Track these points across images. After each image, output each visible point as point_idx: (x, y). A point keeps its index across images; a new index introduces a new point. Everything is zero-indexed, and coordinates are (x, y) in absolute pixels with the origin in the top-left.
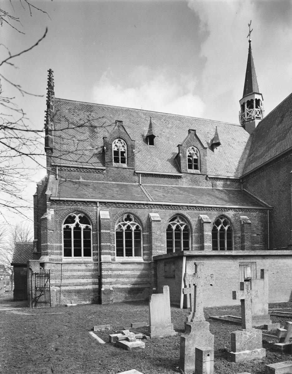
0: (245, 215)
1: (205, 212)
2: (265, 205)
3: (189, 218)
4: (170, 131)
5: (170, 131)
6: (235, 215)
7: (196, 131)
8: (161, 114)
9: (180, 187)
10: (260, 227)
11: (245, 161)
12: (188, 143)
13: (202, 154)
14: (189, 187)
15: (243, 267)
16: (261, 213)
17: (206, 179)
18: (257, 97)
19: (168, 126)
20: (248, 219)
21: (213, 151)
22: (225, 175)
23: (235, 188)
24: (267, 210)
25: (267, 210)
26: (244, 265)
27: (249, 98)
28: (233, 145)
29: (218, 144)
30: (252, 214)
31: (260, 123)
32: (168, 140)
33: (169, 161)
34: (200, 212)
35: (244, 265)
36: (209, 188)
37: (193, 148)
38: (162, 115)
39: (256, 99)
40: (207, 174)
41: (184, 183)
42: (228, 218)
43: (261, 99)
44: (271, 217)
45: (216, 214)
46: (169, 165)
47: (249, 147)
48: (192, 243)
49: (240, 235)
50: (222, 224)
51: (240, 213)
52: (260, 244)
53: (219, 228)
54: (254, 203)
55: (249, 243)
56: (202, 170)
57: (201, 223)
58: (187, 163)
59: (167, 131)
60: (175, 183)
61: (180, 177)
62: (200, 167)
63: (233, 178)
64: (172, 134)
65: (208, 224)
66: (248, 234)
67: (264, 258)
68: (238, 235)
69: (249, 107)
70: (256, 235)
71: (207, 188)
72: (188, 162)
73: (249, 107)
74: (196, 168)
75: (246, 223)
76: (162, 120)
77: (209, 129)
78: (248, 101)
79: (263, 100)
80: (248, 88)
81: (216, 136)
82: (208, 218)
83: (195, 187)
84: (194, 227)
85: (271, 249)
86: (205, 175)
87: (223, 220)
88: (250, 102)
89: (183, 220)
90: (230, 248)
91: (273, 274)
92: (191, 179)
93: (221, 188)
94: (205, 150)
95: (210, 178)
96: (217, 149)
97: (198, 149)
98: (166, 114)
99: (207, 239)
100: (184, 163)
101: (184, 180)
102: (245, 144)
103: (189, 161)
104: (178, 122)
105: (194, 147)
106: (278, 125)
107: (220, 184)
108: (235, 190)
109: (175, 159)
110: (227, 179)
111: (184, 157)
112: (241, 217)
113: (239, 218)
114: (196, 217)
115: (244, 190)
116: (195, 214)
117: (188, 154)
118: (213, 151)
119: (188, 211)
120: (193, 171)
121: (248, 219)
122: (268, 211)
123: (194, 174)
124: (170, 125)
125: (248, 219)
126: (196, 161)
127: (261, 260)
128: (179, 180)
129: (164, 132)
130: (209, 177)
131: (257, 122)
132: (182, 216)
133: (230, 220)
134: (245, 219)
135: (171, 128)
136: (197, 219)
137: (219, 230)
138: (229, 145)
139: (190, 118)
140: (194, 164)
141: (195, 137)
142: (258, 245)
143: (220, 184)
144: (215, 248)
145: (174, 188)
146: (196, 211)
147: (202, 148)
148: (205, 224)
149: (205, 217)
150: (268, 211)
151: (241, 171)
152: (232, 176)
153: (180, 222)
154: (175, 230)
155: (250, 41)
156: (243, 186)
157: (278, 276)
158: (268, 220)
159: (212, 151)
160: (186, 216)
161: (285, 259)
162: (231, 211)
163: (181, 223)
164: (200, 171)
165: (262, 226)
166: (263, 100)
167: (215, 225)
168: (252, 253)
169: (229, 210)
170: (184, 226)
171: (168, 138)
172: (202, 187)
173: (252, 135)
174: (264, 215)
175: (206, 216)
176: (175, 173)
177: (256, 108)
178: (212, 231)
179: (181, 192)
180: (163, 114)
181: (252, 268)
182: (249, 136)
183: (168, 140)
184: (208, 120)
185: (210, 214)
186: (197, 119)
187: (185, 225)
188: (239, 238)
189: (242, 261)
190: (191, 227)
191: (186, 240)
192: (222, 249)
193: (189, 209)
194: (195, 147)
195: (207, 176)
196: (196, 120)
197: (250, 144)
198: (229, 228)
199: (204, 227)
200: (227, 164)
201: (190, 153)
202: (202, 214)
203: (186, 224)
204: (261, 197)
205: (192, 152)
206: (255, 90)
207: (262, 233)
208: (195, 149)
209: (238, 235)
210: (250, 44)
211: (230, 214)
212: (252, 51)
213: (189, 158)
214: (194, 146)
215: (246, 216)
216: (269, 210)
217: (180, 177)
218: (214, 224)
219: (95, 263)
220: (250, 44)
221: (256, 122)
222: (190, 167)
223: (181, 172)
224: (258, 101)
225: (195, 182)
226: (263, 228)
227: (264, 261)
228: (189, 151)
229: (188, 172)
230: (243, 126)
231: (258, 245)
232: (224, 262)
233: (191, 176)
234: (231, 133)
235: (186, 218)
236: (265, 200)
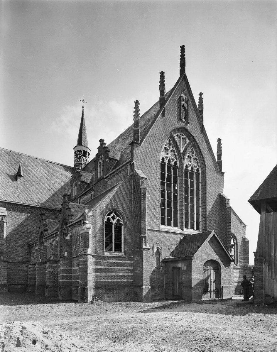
39: (84, 151)
43: (89, 151)
96: (20, 179)
155: (83, 107)
210: (83, 109)
220: (83, 109)
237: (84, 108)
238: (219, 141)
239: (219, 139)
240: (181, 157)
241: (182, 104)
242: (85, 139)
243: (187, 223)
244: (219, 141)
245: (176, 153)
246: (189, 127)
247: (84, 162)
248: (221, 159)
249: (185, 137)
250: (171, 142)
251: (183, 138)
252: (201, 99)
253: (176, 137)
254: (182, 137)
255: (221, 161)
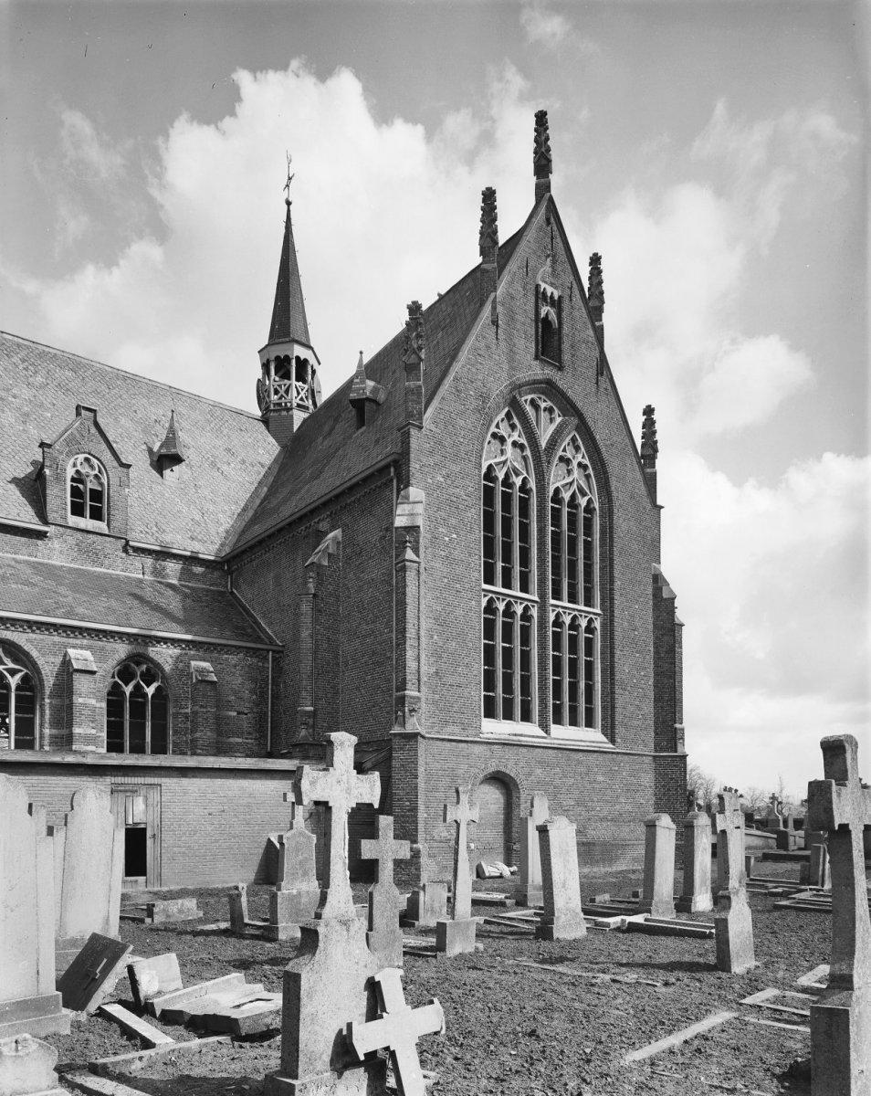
0: (204, 660)
1: (85, 642)
2: (270, 637)
3: (34, 654)
4: (35, 396)
5: (35, 396)
6: (178, 659)
7: (99, 415)
8: (16, 339)
9: (40, 563)
10: (246, 694)
11: (251, 513)
12: (73, 445)
13: (114, 481)
14: (72, 565)
15: (121, 795)
16: (251, 657)
17: (125, 551)
18: (299, 351)
19: (31, 379)
20: (212, 672)
21: (162, 476)
22: (183, 545)
23: (211, 585)
24: (268, 651)
25: (268, 651)
26: (126, 791)
27: (280, 351)
28: (225, 468)
29: (176, 459)
30: (227, 660)
31: (305, 421)
32: (24, 422)
33: (17, 485)
34: (71, 641)
35: (126, 791)
36: (130, 575)
37: (87, 460)
38: (19, 345)
39: (298, 358)
40: (128, 538)
41: (56, 552)
42: (158, 665)
43: (312, 361)
44: (278, 670)
45: (122, 650)
46: (14, 497)
47: (271, 479)
48: (42, 725)
49: (189, 711)
50: (138, 678)
51: (192, 652)
52: (247, 739)
53: (128, 689)
54: (244, 629)
55: (209, 734)
56: (113, 524)
57: (67, 671)
58: (69, 499)
59: (26, 393)
60: (24, 550)
61: (41, 535)
62: (108, 515)
63: (212, 558)
64: (41, 405)
65: (88, 676)
66: (209, 709)
67: (185, 776)
68: (183, 711)
69: (280, 374)
70: (235, 714)
71: (127, 574)
72: (72, 496)
73: (280, 374)
74: (96, 514)
75: (202, 681)
76: (15, 359)
77: (161, 412)
78: (277, 358)
79: (319, 364)
80: (280, 325)
81: (171, 439)
82: (92, 659)
83: (90, 568)
84: (49, 682)
85: (270, 755)
86: (122, 538)
87: (144, 667)
88: (284, 359)
89: (15, 661)
90: (159, 749)
91: (210, 814)
92: (77, 545)
93: (175, 582)
94: (125, 470)
95: (137, 550)
96: (172, 470)
97: (102, 463)
98: (31, 344)
99: (83, 717)
100: (59, 497)
101: (56, 544)
102: (263, 471)
103: (76, 492)
104: (70, 374)
105: (90, 457)
106: (325, 438)
107: (173, 568)
108: (208, 591)
109: (35, 480)
110: (193, 559)
111: (59, 478)
112: (193, 663)
113: (189, 666)
114: (55, 654)
115: (232, 593)
116: (54, 644)
117: (70, 472)
118: (162, 476)
119: (31, 635)
120: (86, 523)
121: (212, 669)
122: (271, 653)
123: (89, 532)
124: (40, 379)
125: (212, 672)
126: (96, 496)
127: (175, 780)
128: (40, 542)
129: (15, 397)
130: (133, 547)
131: (299, 417)
132: (15, 648)
133: (162, 670)
134: (201, 671)
135: (43, 386)
136: (59, 660)
137: (128, 694)
138: (213, 464)
139: (110, 370)
140: (90, 501)
141: (93, 430)
142: (240, 740)
143: (173, 568)
144: (115, 746)
145: (18, 566)
146: (57, 639)
147: (115, 464)
148: (76, 676)
149: (81, 655)
150: (271, 653)
151: (233, 539)
152: (208, 551)
153: (6, 665)
154: (18, 688)
155: (288, 203)
156: (231, 582)
157: (223, 822)
158: (270, 677)
159: (158, 475)
160: (25, 648)
161: (245, 778)
162: (165, 646)
163: (11, 665)
164: (108, 525)
165: (252, 692)
166: (319, 364)
167: (117, 679)
168: (191, 762)
169: (158, 642)
170: (19, 676)
171: (27, 415)
172: (110, 571)
173: (284, 447)
174: (260, 664)
175: (87, 654)
176: (27, 518)
177: (297, 380)
178: (109, 694)
179: (36, 579)
180: (21, 341)
181: (150, 800)
182: (277, 452)
183: (24, 422)
184: (163, 387)
185: (102, 649)
186: (131, 376)
187: (23, 673)
188: (187, 717)
189: (120, 780)
190: (41, 681)
191: (26, 716)
192: (138, 749)
193: (33, 632)
194: (94, 456)
195: (127, 542)
196: (125, 378)
197: (277, 467)
198: (158, 689)
199: (75, 683)
200: (197, 518)
201: (78, 472)
202: (74, 647)
203: (26, 671)
204: (264, 617)
205: (85, 470)
206: (296, 334)
207: (251, 709)
208: (95, 462)
209: (183, 711)
210: (289, 211)
211: (164, 656)
212: (294, 229)
213: (75, 484)
214: (89, 454)
215: (208, 661)
216: (274, 651)
217: (41, 535)
218: (113, 677)
219: (654, 757)
220: (289, 211)
221: (295, 417)
222: (77, 510)
223: (46, 523)
224: (302, 364)
225: (95, 556)
226: (254, 697)
227: (185, 782)
228: (75, 465)
229: (70, 524)
230: (265, 421)
231: (240, 740)
232: (63, 782)
233: (79, 535)
234: (225, 432)
235: (27, 654)
236: (270, 624)
237: (291, 207)
238: (649, 411)
239: (595, 255)
240: (540, 458)
241: (543, 315)
242: (261, 778)
243: (573, 710)
244: (649, 411)
245: (528, 452)
246: (562, 381)
247: (298, 401)
248: (654, 467)
249: (549, 403)
250: (516, 421)
251: (545, 409)
252: (649, 425)
253: (528, 408)
254: (543, 405)
255: (656, 473)
